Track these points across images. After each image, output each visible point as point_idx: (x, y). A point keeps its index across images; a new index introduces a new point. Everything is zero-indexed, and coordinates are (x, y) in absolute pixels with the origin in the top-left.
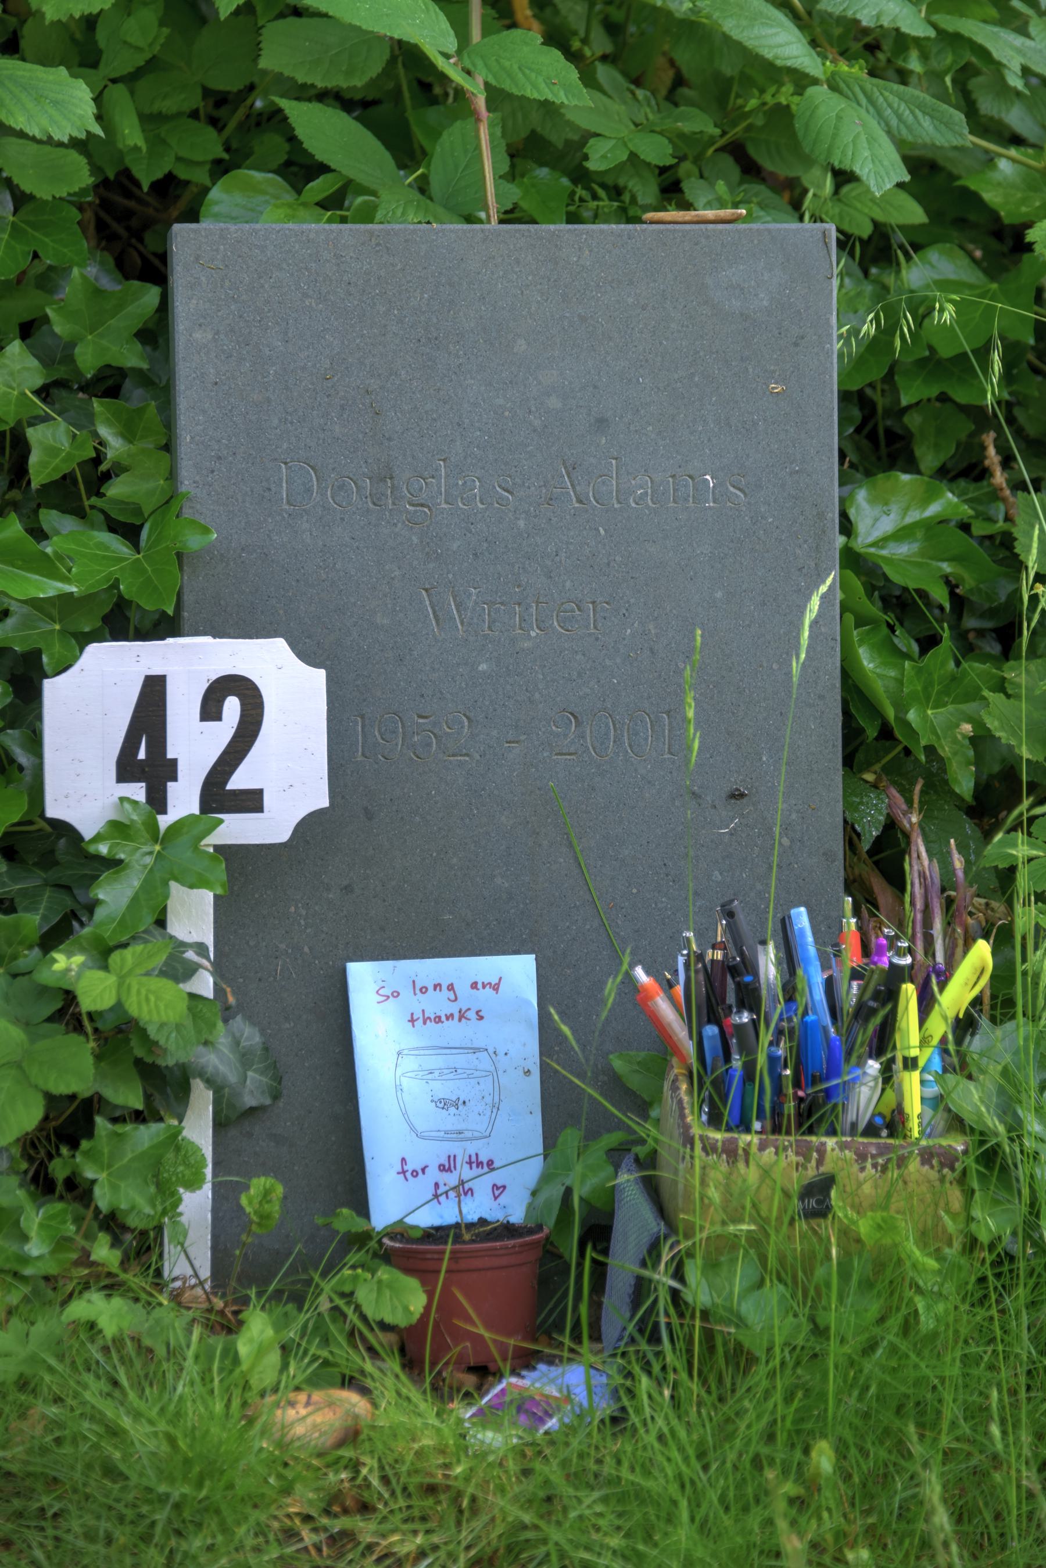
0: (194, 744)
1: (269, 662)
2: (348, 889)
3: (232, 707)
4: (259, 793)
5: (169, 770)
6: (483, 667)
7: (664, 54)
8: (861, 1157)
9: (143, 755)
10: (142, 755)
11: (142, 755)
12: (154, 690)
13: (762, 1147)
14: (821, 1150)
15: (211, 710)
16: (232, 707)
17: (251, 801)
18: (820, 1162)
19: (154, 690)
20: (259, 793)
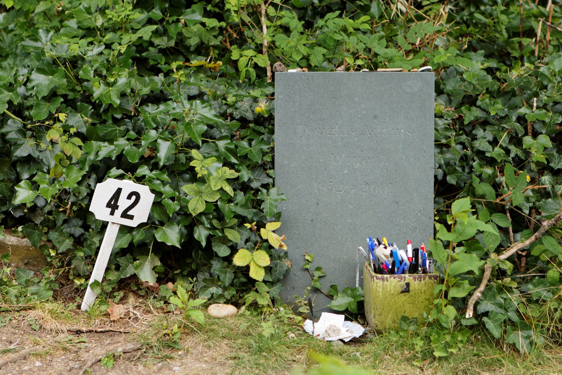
0: (123, 203)
1: (144, 190)
2: (312, 220)
3: (134, 198)
4: (133, 216)
5: (117, 207)
6: (345, 172)
7: (36, 173)
8: (415, 279)
9: (113, 205)
10: (112, 203)
11: (112, 203)
12: (119, 191)
13: (390, 277)
14: (405, 278)
15: (129, 197)
16: (134, 198)
17: (131, 217)
18: (405, 280)
19: (119, 191)
20: (133, 216)
